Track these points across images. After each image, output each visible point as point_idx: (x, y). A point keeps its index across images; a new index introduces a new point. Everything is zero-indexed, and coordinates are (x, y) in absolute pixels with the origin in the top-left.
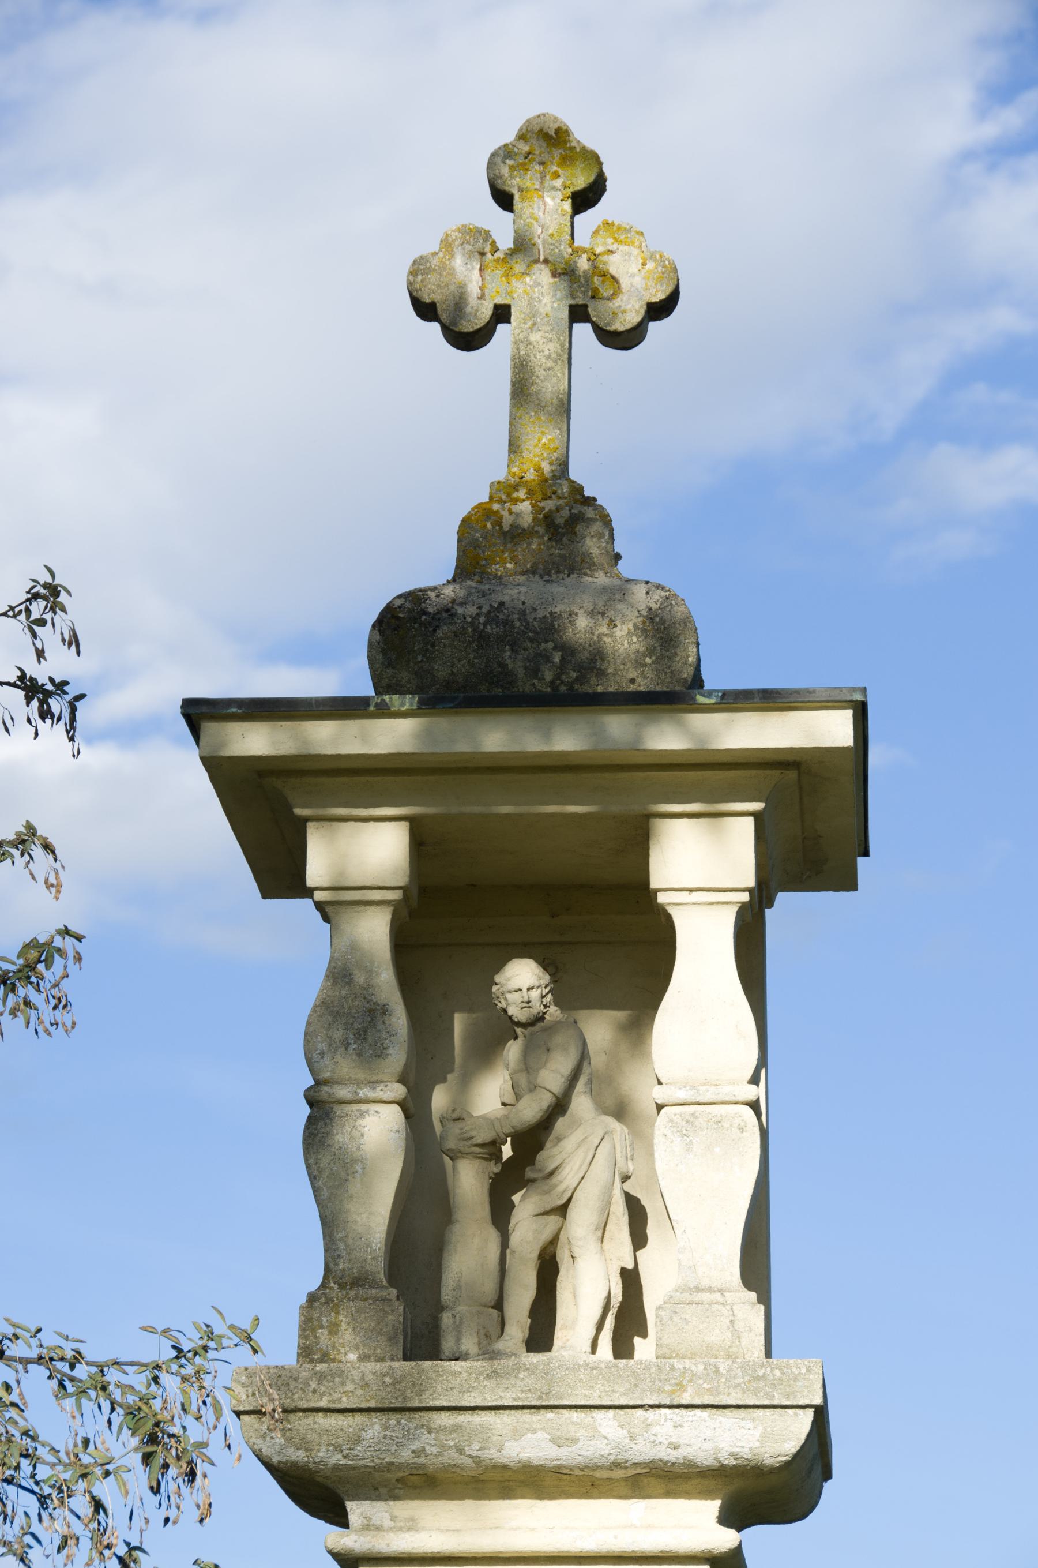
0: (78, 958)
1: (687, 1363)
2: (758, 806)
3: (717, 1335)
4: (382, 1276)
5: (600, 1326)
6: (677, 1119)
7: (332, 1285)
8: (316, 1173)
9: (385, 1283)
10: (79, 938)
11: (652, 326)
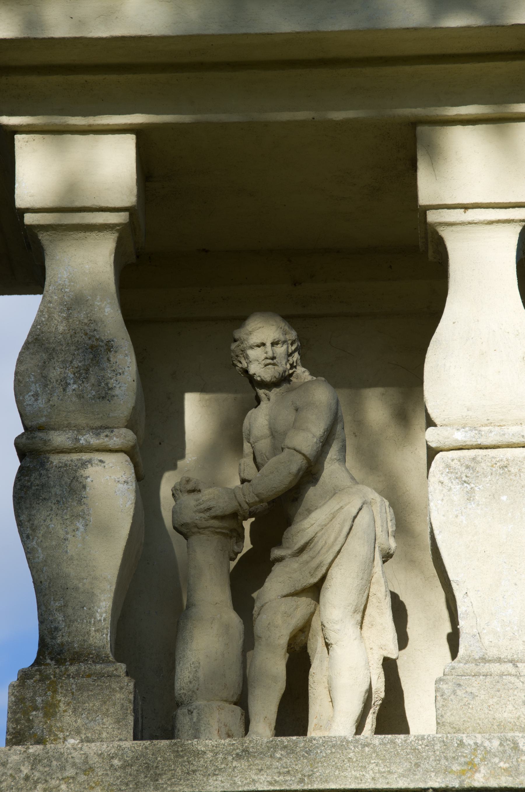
4: (108, 650)
6: (455, 464)
7: (49, 661)
8: (29, 531)
9: (111, 658)
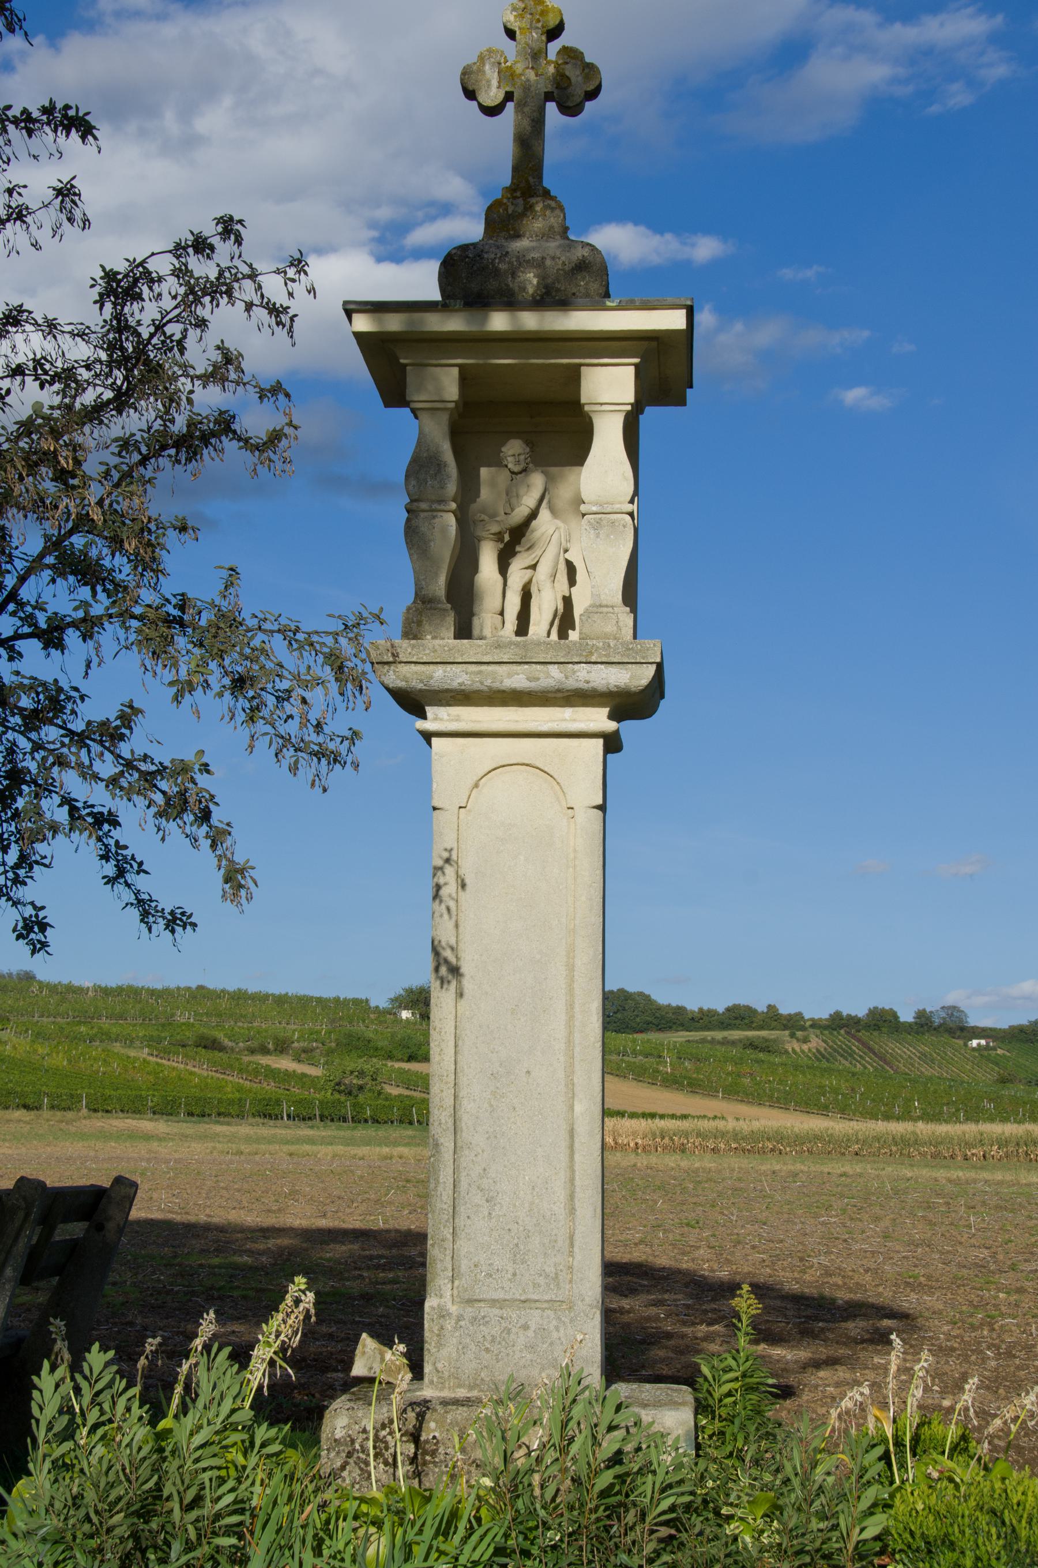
0: (296, 438)
1: (595, 642)
2: (636, 360)
3: (610, 628)
5: (552, 624)
10: (296, 428)
11: (588, 104)
